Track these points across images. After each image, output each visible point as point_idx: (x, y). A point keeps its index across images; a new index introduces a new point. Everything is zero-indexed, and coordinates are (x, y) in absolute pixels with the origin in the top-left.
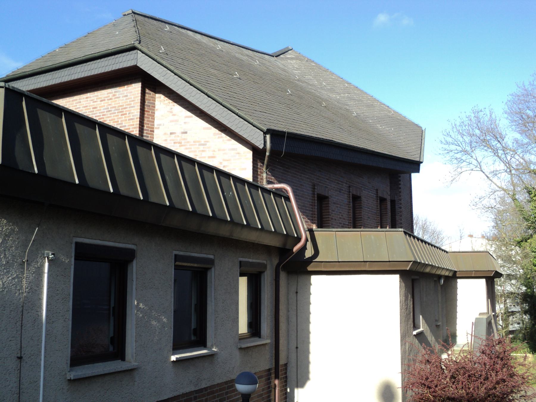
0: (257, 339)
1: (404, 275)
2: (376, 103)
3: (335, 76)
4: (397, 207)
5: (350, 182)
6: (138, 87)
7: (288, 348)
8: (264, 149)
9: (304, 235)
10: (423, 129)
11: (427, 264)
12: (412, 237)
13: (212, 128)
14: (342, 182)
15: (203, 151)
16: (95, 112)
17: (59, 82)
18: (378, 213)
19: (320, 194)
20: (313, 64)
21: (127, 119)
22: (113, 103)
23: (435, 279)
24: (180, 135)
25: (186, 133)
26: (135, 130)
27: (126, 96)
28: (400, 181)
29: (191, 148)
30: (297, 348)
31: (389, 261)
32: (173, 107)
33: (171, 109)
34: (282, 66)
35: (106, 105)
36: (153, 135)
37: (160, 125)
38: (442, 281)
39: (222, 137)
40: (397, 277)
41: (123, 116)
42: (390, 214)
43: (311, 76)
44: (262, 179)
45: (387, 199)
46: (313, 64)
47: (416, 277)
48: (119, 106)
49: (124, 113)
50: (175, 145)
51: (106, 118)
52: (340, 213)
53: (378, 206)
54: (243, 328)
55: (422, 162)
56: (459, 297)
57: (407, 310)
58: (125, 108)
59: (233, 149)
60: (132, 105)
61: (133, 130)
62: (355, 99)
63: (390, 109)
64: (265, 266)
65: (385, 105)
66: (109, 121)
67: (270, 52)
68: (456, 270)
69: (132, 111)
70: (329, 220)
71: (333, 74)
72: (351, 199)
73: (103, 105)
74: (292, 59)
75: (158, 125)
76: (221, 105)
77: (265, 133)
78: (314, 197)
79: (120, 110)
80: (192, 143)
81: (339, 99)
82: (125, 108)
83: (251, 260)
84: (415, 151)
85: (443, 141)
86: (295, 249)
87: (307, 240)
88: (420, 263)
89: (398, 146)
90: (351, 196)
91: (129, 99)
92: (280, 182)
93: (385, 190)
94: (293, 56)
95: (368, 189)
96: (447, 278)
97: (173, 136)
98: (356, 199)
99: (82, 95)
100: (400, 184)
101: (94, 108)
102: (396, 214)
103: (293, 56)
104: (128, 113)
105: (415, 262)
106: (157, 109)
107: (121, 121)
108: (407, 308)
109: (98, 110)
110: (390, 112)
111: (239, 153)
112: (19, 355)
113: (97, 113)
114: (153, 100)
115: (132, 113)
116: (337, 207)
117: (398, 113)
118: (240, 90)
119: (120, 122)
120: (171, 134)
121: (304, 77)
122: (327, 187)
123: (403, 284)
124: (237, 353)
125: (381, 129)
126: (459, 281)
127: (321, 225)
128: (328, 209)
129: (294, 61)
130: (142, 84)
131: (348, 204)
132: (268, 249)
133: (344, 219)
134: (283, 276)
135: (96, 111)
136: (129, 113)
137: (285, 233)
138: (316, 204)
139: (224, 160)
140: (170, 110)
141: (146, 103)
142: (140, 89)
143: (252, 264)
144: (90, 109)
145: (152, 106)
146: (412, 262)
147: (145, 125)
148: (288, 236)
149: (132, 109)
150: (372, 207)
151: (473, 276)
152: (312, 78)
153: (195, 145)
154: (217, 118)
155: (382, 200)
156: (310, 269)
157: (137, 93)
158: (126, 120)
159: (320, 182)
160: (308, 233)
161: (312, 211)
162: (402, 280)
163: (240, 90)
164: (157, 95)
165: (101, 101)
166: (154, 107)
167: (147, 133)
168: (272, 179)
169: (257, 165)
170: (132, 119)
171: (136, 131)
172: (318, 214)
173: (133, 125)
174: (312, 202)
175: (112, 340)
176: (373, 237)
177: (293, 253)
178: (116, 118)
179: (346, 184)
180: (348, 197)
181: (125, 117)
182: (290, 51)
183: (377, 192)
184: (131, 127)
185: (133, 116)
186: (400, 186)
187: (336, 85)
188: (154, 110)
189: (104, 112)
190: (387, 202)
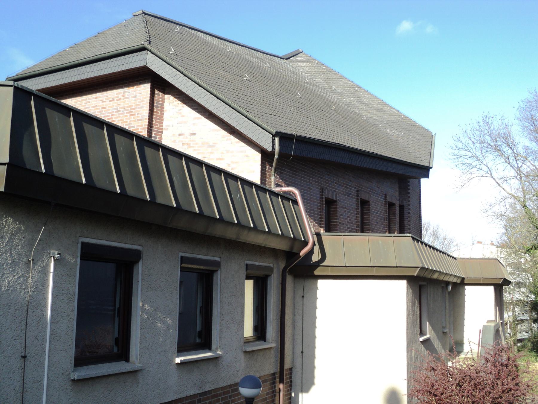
0: (262, 342)
1: (411, 280)
2: (386, 108)
5: (358, 187)
8: (273, 153)
10: (433, 134)
14: (350, 186)
19: (328, 198)
23: (443, 285)
25: (194, 134)
27: (135, 97)
28: (409, 186)
30: (302, 352)
31: (397, 267)
33: (180, 110)
36: (162, 136)
38: (450, 288)
40: (404, 283)
41: (132, 117)
43: (321, 79)
44: (270, 182)
48: (128, 107)
52: (348, 217)
53: (386, 211)
54: (248, 331)
55: (431, 168)
63: (400, 113)
64: (271, 270)
65: (395, 109)
66: (118, 121)
68: (464, 277)
69: (141, 112)
70: (337, 225)
71: (343, 77)
74: (302, 61)
75: (166, 126)
76: (230, 107)
77: (274, 136)
78: (322, 201)
83: (257, 264)
86: (303, 253)
87: (314, 244)
88: (427, 269)
90: (359, 201)
91: (138, 99)
92: (288, 185)
93: (393, 195)
94: (303, 59)
96: (455, 285)
97: (182, 137)
98: (364, 204)
104: (136, 113)
105: (423, 268)
106: (166, 110)
108: (413, 315)
110: (400, 116)
112: (23, 354)
116: (345, 211)
117: (408, 117)
119: (128, 123)
120: (180, 135)
121: (315, 80)
122: (335, 191)
123: (410, 290)
124: (242, 356)
127: (329, 229)
128: (336, 213)
129: (305, 64)
131: (356, 209)
132: (274, 253)
133: (352, 223)
134: (289, 279)
136: (138, 114)
138: (324, 208)
141: (155, 104)
145: (161, 107)
146: (419, 268)
151: (481, 283)
155: (391, 205)
156: (317, 272)
158: (134, 121)
160: (315, 236)
161: (320, 215)
165: (110, 101)
166: (163, 108)
167: (155, 134)
169: (265, 167)
170: (140, 120)
174: (320, 206)
175: (117, 341)
176: (380, 242)
177: (300, 257)
179: (355, 188)
180: (356, 201)
182: (300, 54)
183: (386, 197)
186: (409, 191)
188: (163, 111)
189: (113, 112)
190: (395, 207)
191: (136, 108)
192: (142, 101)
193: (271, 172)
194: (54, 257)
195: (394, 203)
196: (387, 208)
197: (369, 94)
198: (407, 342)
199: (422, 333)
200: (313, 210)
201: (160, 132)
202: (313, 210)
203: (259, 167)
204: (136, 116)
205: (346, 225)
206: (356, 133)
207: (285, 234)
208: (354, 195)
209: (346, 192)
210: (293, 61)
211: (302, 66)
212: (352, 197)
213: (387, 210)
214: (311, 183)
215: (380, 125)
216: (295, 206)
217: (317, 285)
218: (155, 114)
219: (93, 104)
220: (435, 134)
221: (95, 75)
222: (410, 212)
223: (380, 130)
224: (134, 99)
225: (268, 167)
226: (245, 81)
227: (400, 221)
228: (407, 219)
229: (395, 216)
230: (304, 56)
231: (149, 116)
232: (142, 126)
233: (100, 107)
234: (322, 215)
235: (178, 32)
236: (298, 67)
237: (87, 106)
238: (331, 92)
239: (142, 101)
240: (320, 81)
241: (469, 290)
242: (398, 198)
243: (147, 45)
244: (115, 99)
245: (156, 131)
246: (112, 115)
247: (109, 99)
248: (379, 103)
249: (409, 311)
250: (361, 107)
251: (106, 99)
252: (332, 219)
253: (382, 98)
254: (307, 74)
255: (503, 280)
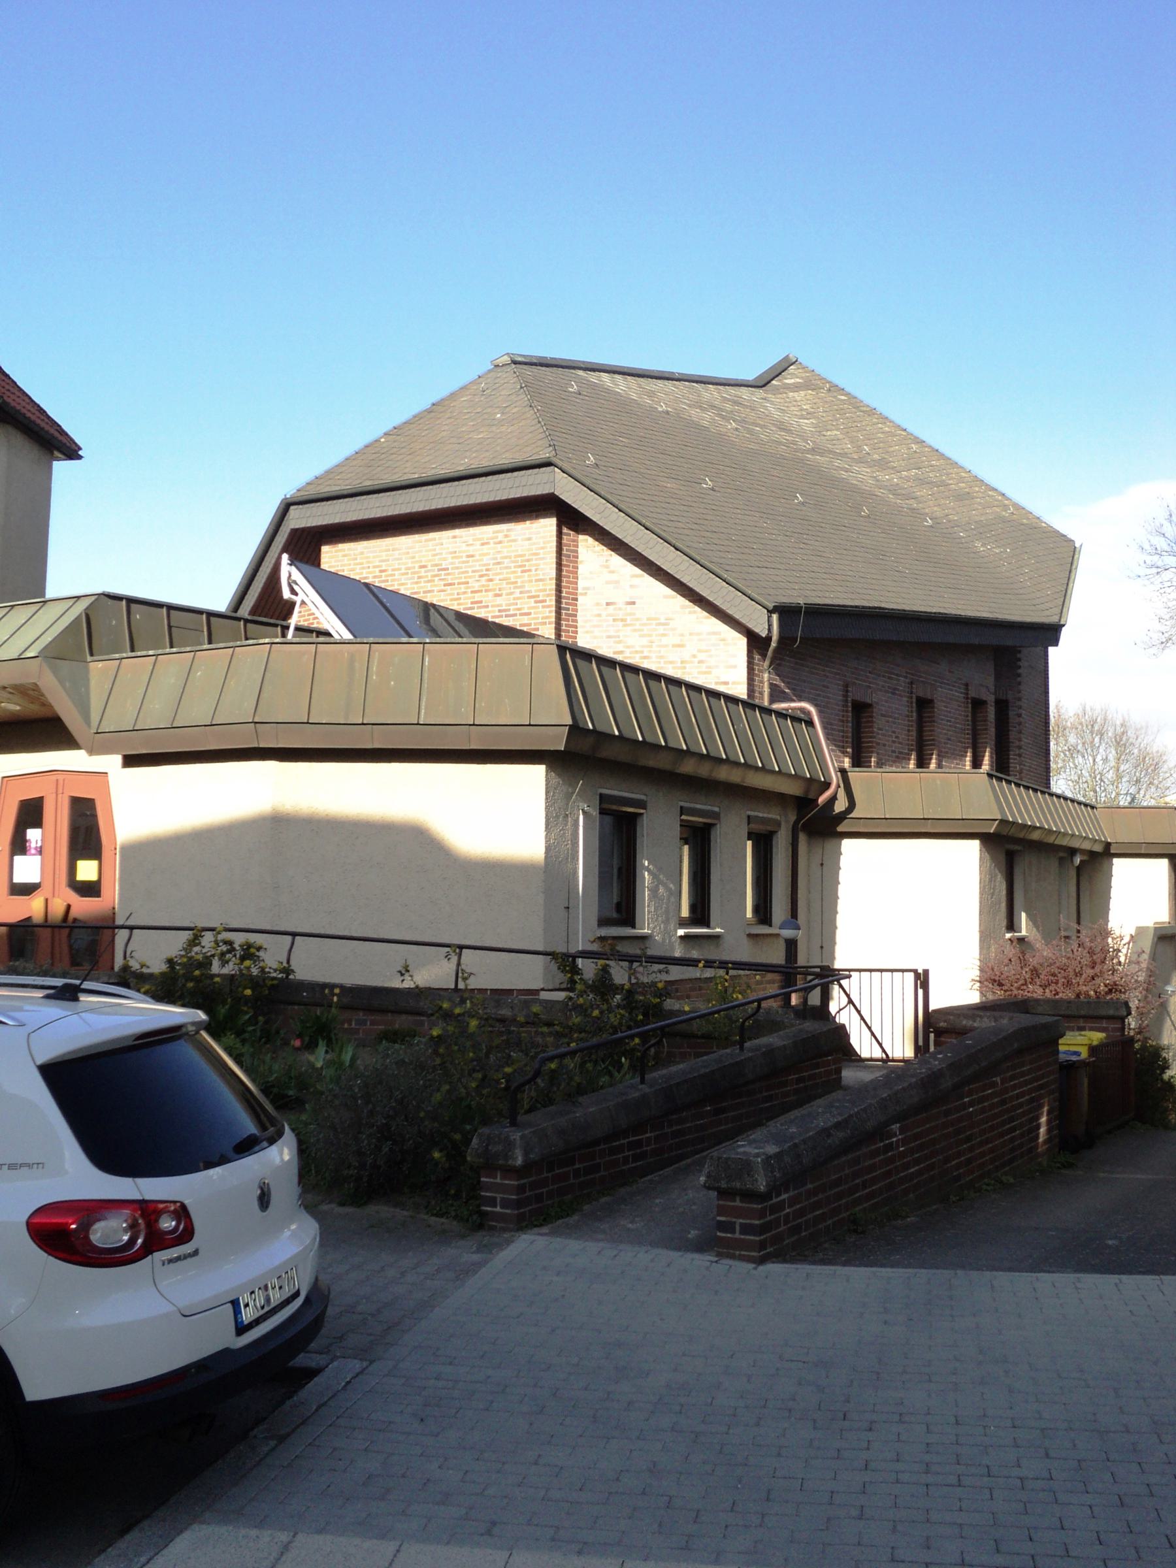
0: (767, 927)
1: (987, 840)
2: (977, 489)
3: (891, 424)
4: (1011, 713)
5: (912, 674)
6: (551, 525)
7: (809, 954)
9: (835, 778)
10: (1077, 545)
11: (1030, 826)
12: (1004, 783)
13: (679, 596)
14: (897, 675)
15: (664, 635)
16: (470, 564)
17: (408, 511)
18: (968, 729)
19: (856, 701)
20: (843, 397)
21: (534, 579)
22: (505, 550)
23: (1061, 854)
24: (624, 606)
25: (634, 603)
26: (548, 599)
27: (529, 539)
28: (1019, 660)
29: (643, 630)
30: (822, 947)
31: (363, 724)
32: (609, 558)
33: (607, 561)
34: (776, 414)
35: (491, 551)
36: (576, 605)
37: (588, 589)
38: (1077, 860)
39: (695, 612)
40: (976, 844)
41: (526, 574)
42: (993, 730)
43: (837, 430)
44: (762, 682)
45: (989, 702)
46: (843, 397)
47: (1017, 847)
48: (516, 556)
49: (527, 568)
50: (615, 623)
51: (493, 575)
52: (894, 732)
53: (967, 716)
55: (1064, 625)
56: (1114, 893)
57: (994, 897)
58: (528, 560)
59: (714, 633)
60: (541, 556)
61: (545, 598)
62: (932, 482)
63: (1008, 499)
64: (779, 824)
65: (996, 490)
66: (500, 580)
67: (750, 375)
68: (1109, 840)
69: (542, 566)
70: (871, 747)
71: (885, 419)
72: (914, 705)
73: (485, 551)
74: (796, 388)
75: (584, 589)
76: (699, 563)
77: (770, 612)
78: (847, 706)
79: (520, 564)
80: (645, 621)
81: (898, 484)
82: (528, 560)
83: (761, 815)
84: (1051, 601)
85: (1147, 546)
86: (822, 799)
87: (839, 786)
88: (1013, 823)
89: (1016, 591)
90: (914, 700)
91: (534, 544)
92: (800, 700)
93: (983, 682)
94: (798, 380)
95: (948, 684)
96: (1093, 855)
97: (611, 607)
98: (924, 705)
99: (444, 532)
100: (1020, 667)
101: (468, 556)
102: (1010, 728)
103: (798, 380)
104: (533, 568)
105: (1003, 822)
106: (581, 562)
107: (522, 582)
108: (993, 894)
109: (477, 561)
110: (1006, 507)
111: (724, 640)
112: (567, 905)
113: (475, 566)
114: (574, 546)
115: (542, 569)
116: (888, 722)
117: (1024, 509)
118: (680, 448)
119: (519, 584)
120: (608, 604)
121: (825, 433)
122: (870, 687)
124: (745, 940)
125: (984, 551)
126: (1116, 861)
127: (858, 762)
128: (871, 727)
129: (802, 393)
130: (558, 520)
131: (908, 716)
132: (781, 798)
133: (900, 743)
134: (802, 838)
135: (473, 561)
136: (536, 570)
137: (808, 776)
138: (850, 719)
139: (699, 651)
140: (605, 564)
141: (564, 552)
142: (554, 528)
143: (764, 821)
144: (462, 557)
145: (574, 557)
146: (997, 822)
147: (564, 590)
148: (812, 781)
149: (542, 562)
150: (956, 718)
151: (1143, 852)
152: (841, 436)
153: (650, 624)
154: (691, 585)
155: (977, 704)
156: (840, 829)
157: (549, 534)
158: (531, 581)
159: (857, 679)
160: (839, 774)
161: (843, 731)
162: (984, 849)
163: (680, 448)
164: (581, 537)
165: (483, 544)
166: (577, 557)
167: (566, 603)
168: (776, 680)
169: (753, 658)
170: (541, 580)
171: (551, 600)
172: (853, 741)
173: (545, 590)
174: (843, 716)
175: (618, 905)
176: (938, 782)
177: (818, 805)
178: (512, 576)
179: (906, 677)
180: (908, 701)
181: (529, 576)
182: (791, 367)
183: (967, 689)
184: (541, 594)
185: (543, 574)
186: (1020, 671)
187: (892, 449)
188: (577, 562)
189: (489, 565)
190: (987, 708)
191: (531, 560)
192: (542, 548)
193: (763, 666)
194: (582, 810)
195: (984, 699)
196: (970, 709)
197: (942, 456)
198: (981, 932)
199: (1011, 926)
200: (831, 724)
201: (573, 599)
202: (831, 724)
203: (745, 658)
204: (533, 572)
205: (889, 746)
206: (909, 569)
207: (784, 771)
208: (904, 691)
209: (889, 687)
210: (777, 388)
211: (796, 401)
212: (900, 695)
213: (970, 714)
214: (827, 677)
215: (961, 534)
216: (809, 728)
217: (840, 848)
218: (564, 568)
219: (448, 548)
220: (1081, 546)
221: (459, 504)
222: (1021, 714)
223: (961, 546)
224: (527, 543)
225: (757, 657)
226: (708, 492)
227: (997, 735)
228: (1015, 727)
229: (987, 725)
230: (800, 371)
231: (557, 575)
232: (545, 590)
233: (464, 555)
234: (847, 732)
235: (574, 392)
236: (790, 405)
237: (437, 552)
238: (860, 461)
239: (542, 548)
240: (836, 435)
241: (1120, 866)
242: (992, 688)
243: (554, 460)
244: (491, 541)
245: (568, 598)
246: (487, 570)
247: (478, 539)
248: (962, 480)
249: (984, 887)
250: (922, 492)
251: (474, 540)
252: (864, 737)
253: (968, 466)
254: (808, 419)
255: (998, 825)
